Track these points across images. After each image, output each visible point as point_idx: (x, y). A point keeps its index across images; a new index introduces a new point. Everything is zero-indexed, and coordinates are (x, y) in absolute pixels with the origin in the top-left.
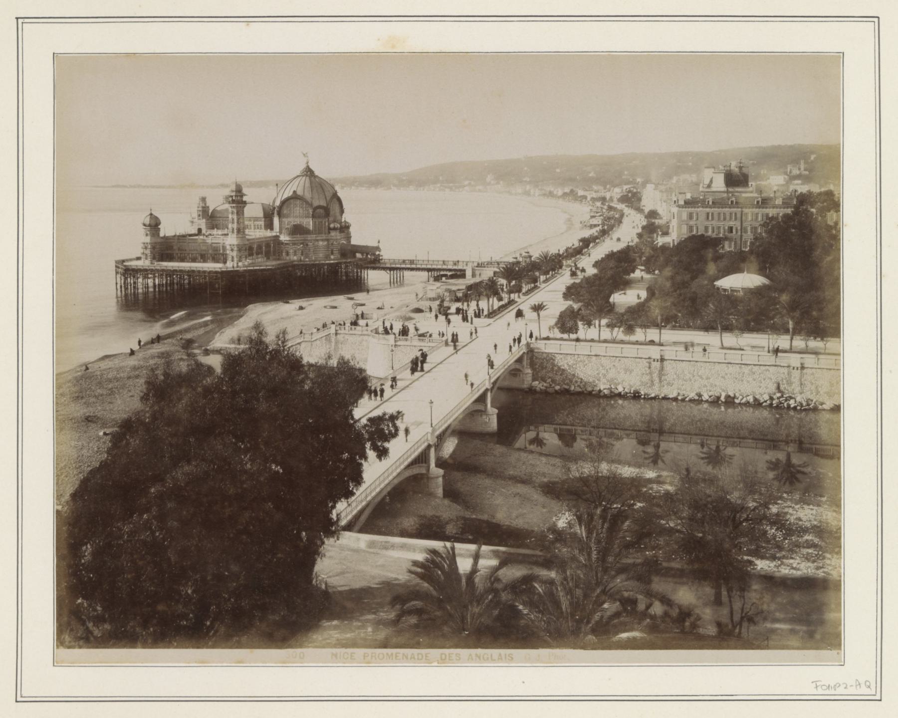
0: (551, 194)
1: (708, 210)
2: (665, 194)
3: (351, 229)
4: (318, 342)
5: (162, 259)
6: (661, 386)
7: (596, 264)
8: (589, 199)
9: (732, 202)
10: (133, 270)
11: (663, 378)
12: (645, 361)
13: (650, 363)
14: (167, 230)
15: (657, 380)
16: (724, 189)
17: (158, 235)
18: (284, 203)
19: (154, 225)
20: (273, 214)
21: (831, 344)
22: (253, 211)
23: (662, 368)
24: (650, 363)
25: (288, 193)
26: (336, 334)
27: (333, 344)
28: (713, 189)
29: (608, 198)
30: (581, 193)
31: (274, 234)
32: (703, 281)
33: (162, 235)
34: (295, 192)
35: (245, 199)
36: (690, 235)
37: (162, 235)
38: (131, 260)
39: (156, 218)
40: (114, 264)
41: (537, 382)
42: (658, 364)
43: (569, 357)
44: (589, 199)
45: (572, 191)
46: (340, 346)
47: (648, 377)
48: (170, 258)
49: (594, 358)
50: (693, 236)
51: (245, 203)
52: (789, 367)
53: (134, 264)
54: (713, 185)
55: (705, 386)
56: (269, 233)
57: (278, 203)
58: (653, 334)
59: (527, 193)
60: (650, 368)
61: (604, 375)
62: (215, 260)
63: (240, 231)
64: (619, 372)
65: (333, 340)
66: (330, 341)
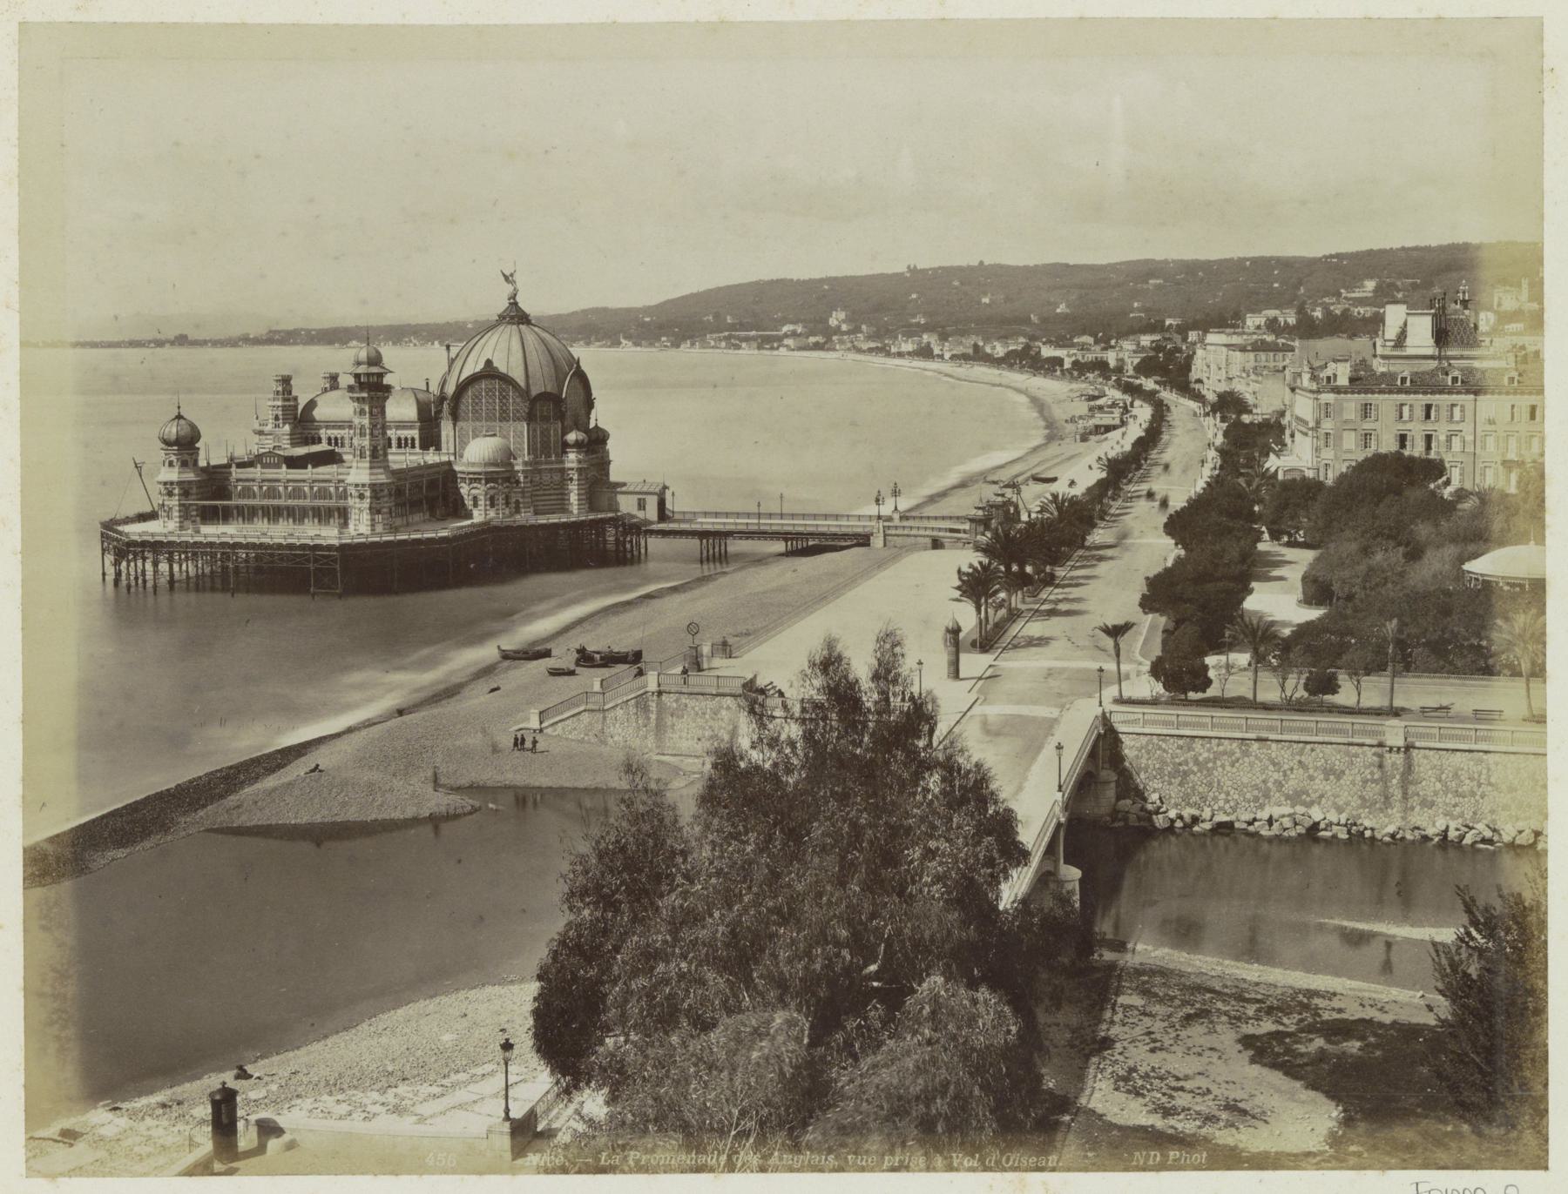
0: (978, 356)
1: (1402, 397)
2: (1252, 355)
3: (610, 445)
4: (619, 712)
5: (210, 515)
6: (1407, 810)
7: (1178, 526)
8: (1067, 365)
9: (1455, 379)
10: (144, 544)
11: (1411, 789)
12: (1369, 752)
13: (1381, 756)
14: (211, 453)
15: (1398, 794)
16: (1431, 350)
17: (196, 462)
18: (462, 388)
19: (185, 445)
20: (439, 412)
21: (1501, 695)
22: (401, 409)
23: (1409, 766)
24: (1381, 756)
25: (473, 366)
26: (660, 693)
27: (653, 716)
28: (1410, 351)
29: (1112, 363)
30: (1048, 352)
31: (445, 458)
32: (1435, 564)
33: (202, 463)
34: (489, 363)
35: (387, 380)
36: (1369, 453)
37: (202, 463)
38: (128, 521)
39: (193, 427)
40: (99, 529)
41: (1129, 802)
42: (1398, 759)
43: (1198, 744)
44: (1067, 365)
45: (1027, 347)
46: (669, 720)
47: (1378, 788)
48: (225, 515)
49: (1256, 746)
50: (1429, 461)
51: (388, 389)
52: (1381, 745)
53: (135, 530)
54: (1409, 341)
55: (1506, 807)
56: (432, 457)
57: (450, 389)
58: (1373, 691)
59: (925, 353)
60: (1381, 766)
61: (1279, 784)
62: (322, 515)
63: (377, 455)
64: (1311, 778)
65: (653, 706)
66: (646, 709)
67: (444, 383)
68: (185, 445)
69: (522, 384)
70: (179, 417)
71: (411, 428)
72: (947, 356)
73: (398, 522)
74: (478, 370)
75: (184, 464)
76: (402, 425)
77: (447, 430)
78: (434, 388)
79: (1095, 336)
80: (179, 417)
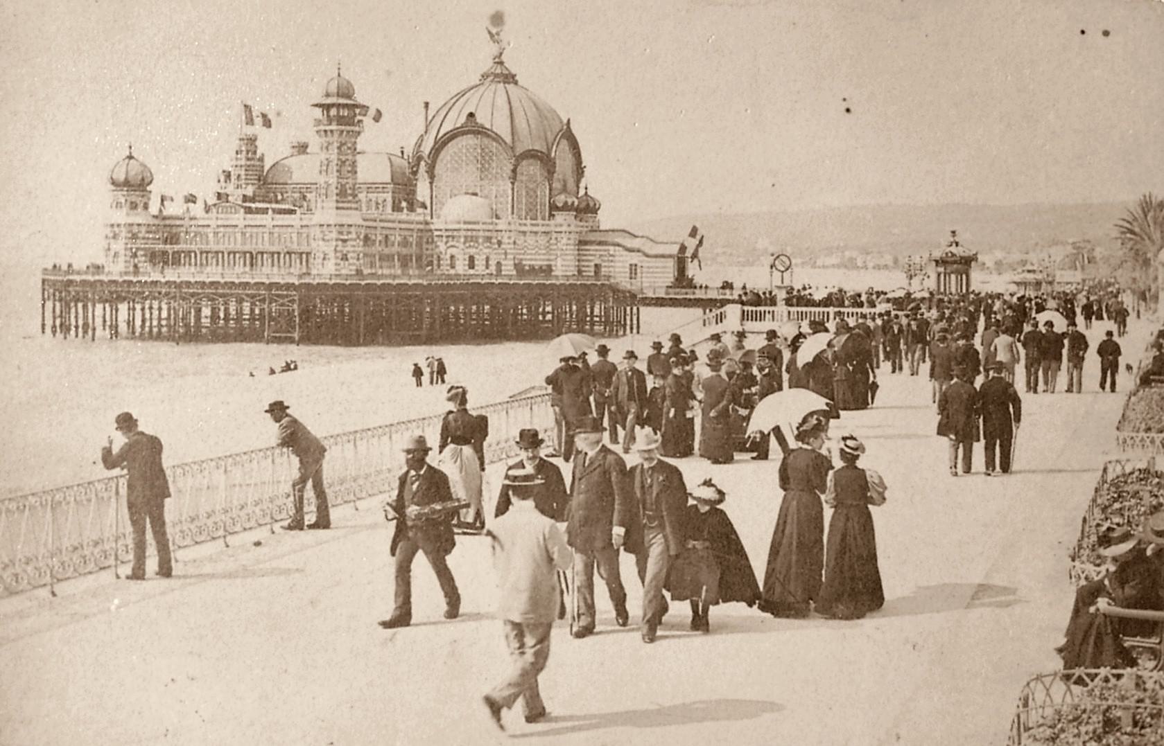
18: (441, 144)
19: (134, 186)
48: (176, 260)
67: (419, 144)
68: (134, 186)
69: (508, 140)
70: (130, 157)
71: (384, 190)
72: (871, 265)
73: (354, 336)
74: (458, 125)
75: (134, 206)
76: (372, 187)
77: (422, 191)
78: (409, 151)
79: (677, 556)
80: (130, 157)
